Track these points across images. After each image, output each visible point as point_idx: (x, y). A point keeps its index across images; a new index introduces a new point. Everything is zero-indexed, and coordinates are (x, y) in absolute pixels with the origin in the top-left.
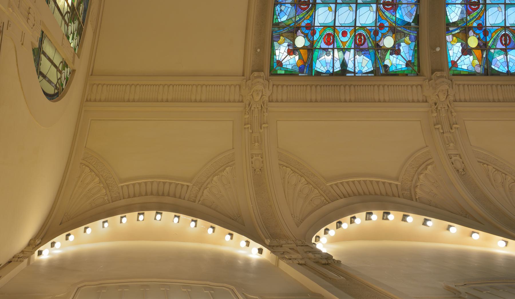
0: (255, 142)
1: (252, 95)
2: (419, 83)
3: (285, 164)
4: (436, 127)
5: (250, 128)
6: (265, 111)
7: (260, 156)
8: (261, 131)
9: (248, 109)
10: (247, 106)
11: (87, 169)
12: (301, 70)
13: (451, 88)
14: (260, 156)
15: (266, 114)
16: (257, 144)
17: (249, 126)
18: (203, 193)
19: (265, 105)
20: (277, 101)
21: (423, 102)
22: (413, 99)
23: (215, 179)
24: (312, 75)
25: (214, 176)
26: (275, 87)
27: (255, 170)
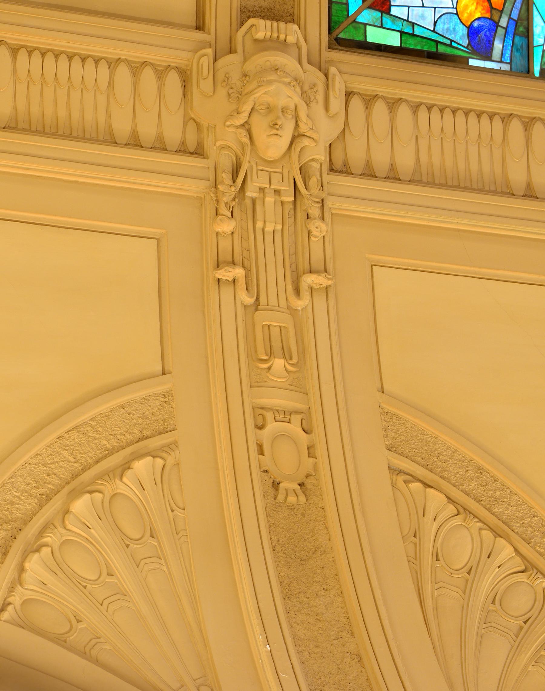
0: (271, 353)
1: (246, 126)
2: (179, 58)
3: (419, 471)
4: (221, 274)
5: (242, 282)
6: (315, 211)
7: (296, 419)
8: (300, 304)
9: (228, 191)
10: (226, 178)
11: (435, 499)
12: (480, 40)
13: (318, 108)
14: (296, 419)
15: (319, 229)
16: (279, 363)
17: (239, 272)
18: (21, 569)
19: (313, 182)
20: (369, 173)
21: (182, 150)
22: (392, 167)
23: (81, 506)
24: (528, 71)
25: (75, 494)
26: (356, 103)
27: (276, 485)
